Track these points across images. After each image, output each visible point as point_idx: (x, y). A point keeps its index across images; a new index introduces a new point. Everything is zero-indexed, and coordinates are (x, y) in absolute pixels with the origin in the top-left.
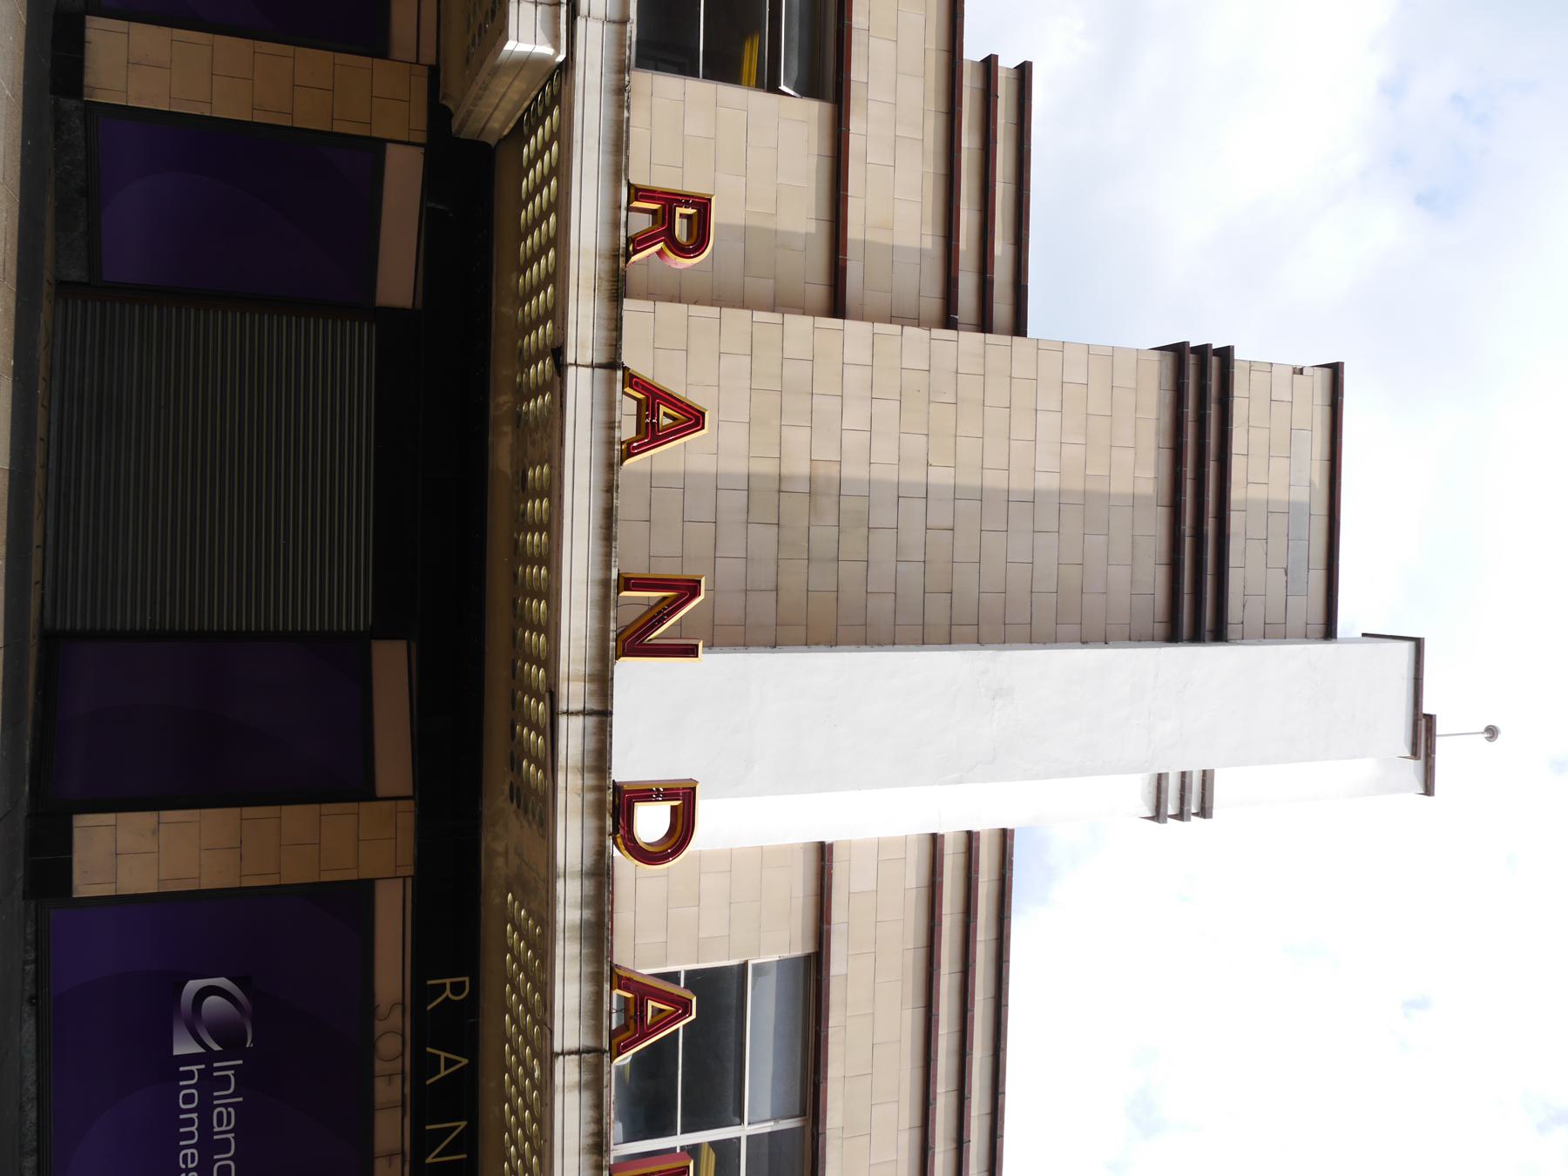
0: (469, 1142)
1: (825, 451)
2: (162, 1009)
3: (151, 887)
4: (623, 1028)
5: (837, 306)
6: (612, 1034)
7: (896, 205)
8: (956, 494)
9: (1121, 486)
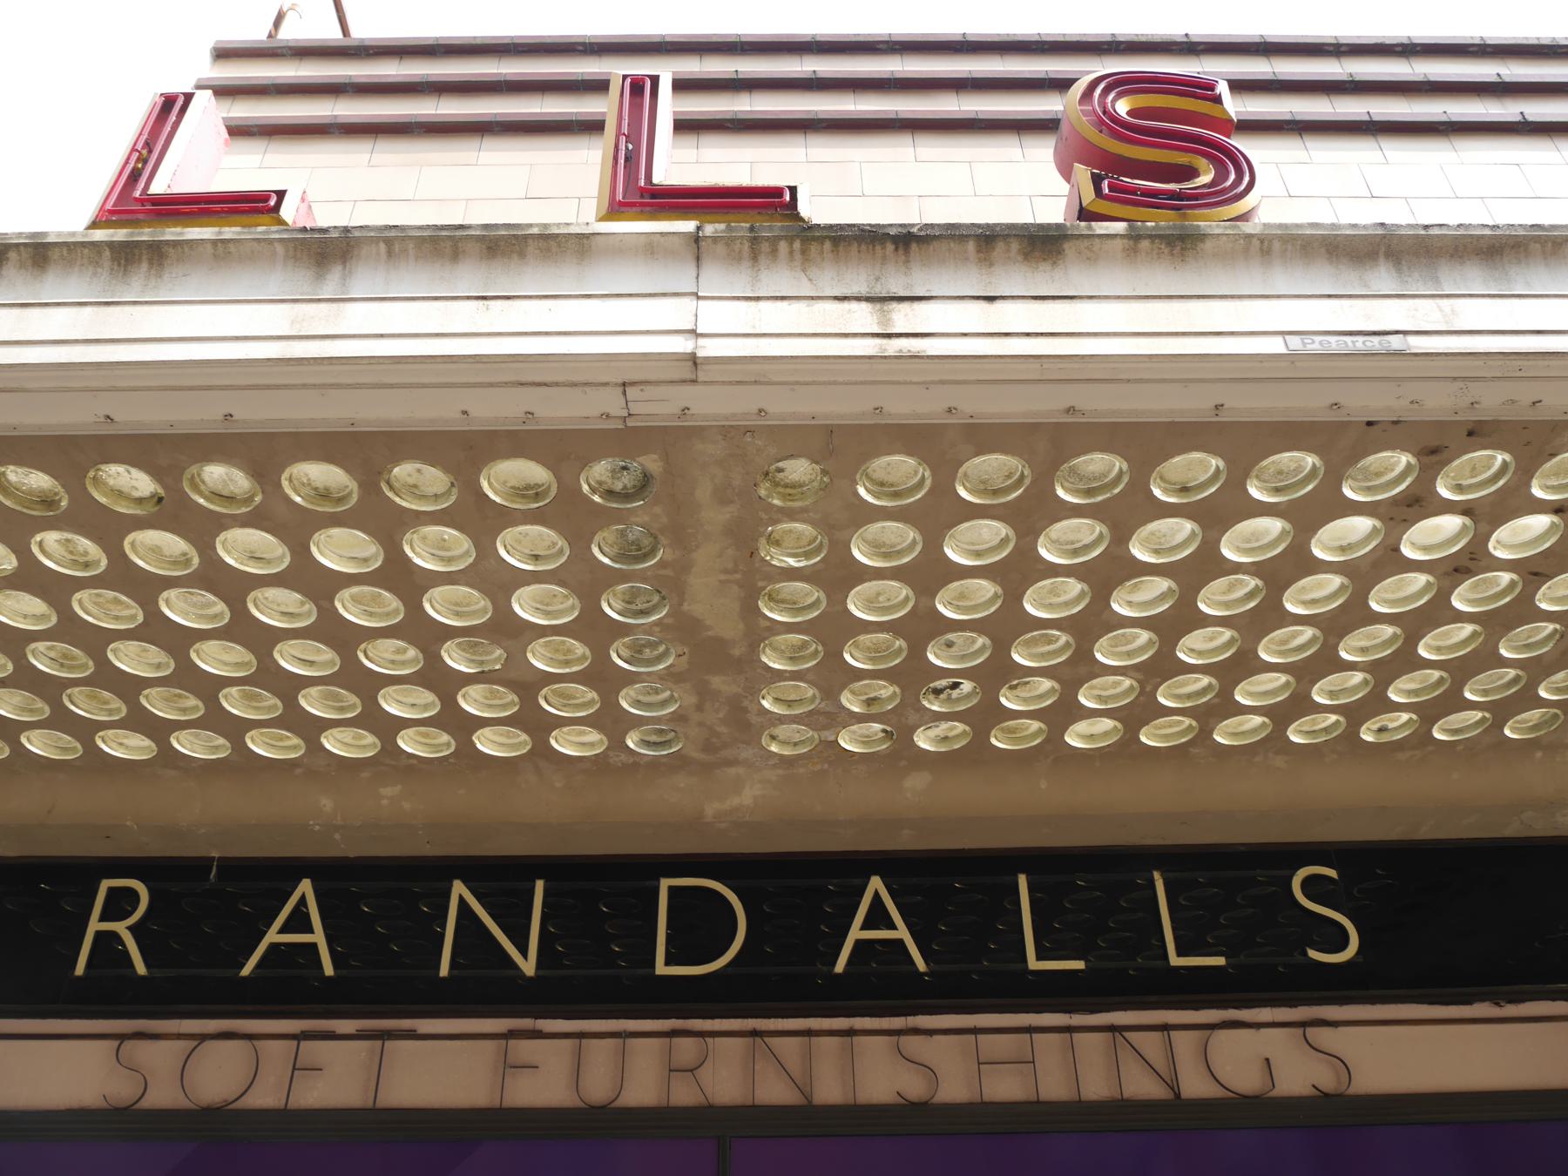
0: (502, 879)
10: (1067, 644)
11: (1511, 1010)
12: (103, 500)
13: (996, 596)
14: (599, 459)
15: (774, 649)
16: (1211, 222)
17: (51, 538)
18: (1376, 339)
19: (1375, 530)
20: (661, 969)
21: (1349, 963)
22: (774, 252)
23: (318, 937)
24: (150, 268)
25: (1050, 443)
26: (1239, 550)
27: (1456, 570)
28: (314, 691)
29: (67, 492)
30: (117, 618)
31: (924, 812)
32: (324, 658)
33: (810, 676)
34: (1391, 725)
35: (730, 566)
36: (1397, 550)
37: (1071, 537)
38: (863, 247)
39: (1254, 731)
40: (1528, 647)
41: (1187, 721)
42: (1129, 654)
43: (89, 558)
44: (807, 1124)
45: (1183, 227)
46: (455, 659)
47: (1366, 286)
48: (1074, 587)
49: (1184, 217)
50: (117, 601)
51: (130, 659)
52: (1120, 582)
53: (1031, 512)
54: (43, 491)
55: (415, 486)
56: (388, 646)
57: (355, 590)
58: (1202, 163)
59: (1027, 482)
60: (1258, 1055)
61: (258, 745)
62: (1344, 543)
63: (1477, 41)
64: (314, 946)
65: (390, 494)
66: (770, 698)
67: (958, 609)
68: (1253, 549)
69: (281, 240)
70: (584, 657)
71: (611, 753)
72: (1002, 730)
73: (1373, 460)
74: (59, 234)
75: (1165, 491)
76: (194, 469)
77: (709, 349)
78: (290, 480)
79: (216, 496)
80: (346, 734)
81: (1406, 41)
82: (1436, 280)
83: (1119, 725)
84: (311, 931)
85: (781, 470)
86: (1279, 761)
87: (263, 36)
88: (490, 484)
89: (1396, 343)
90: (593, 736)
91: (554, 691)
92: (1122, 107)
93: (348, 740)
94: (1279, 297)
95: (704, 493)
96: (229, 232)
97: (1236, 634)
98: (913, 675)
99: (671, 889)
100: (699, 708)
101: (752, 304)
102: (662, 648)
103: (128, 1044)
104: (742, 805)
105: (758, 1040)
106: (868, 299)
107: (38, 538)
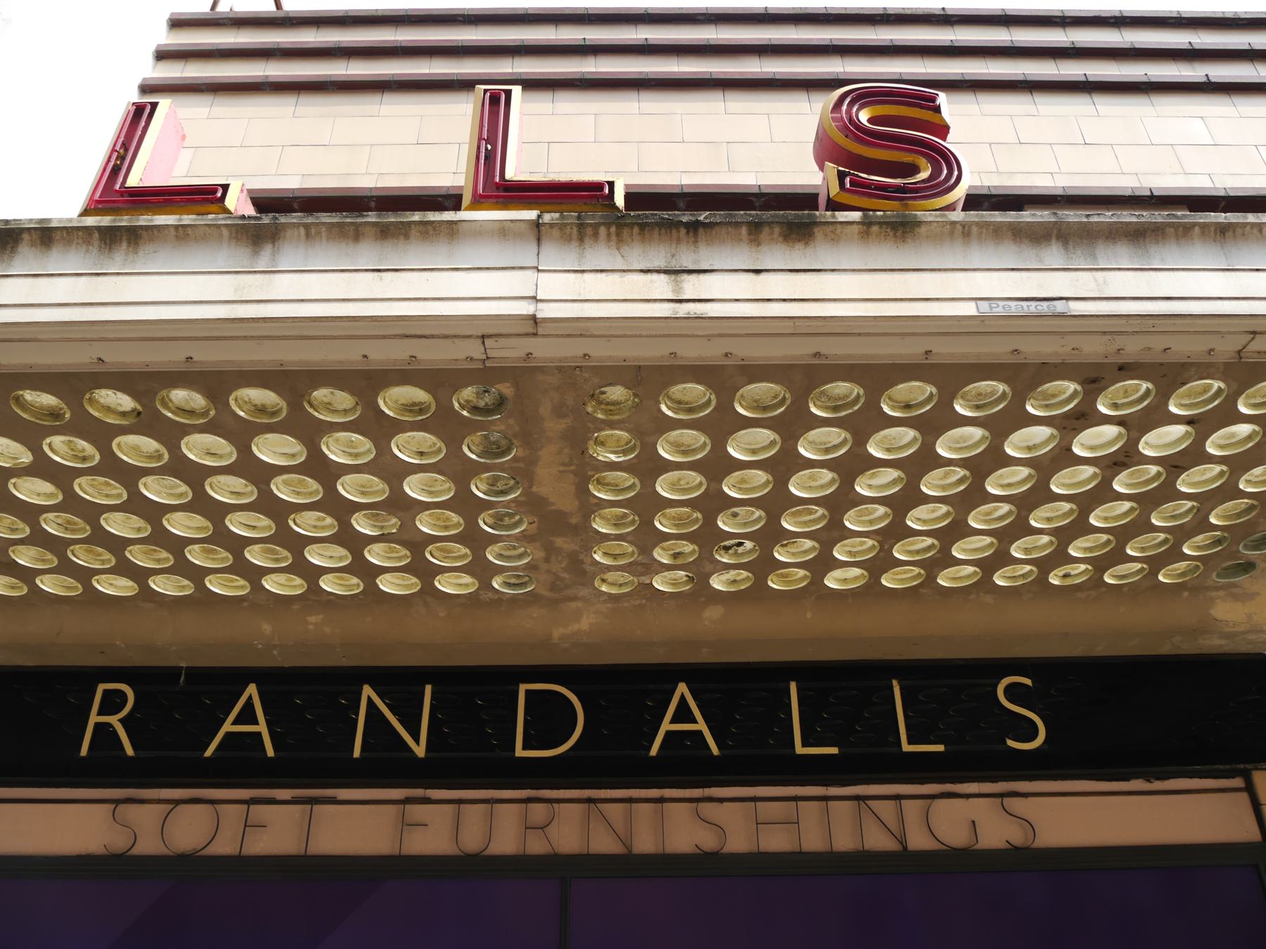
0: (400, 683)
10: (823, 516)
11: (1158, 785)
12: (96, 414)
13: (768, 482)
14: (466, 386)
15: (603, 518)
16: (925, 212)
17: (58, 440)
18: (1045, 304)
19: (1052, 437)
20: (520, 752)
21: (1037, 749)
22: (596, 235)
23: (262, 727)
24: (129, 246)
25: (805, 377)
26: (951, 449)
27: (1115, 464)
28: (257, 547)
29: (69, 408)
30: (107, 496)
31: (718, 635)
32: (264, 525)
33: (629, 538)
34: (1073, 573)
35: (567, 461)
36: (1070, 450)
37: (824, 439)
38: (663, 231)
39: (968, 576)
40: (1174, 517)
41: (917, 570)
42: (871, 522)
43: (86, 454)
44: (628, 867)
45: (904, 216)
46: (361, 524)
47: (1041, 261)
48: (827, 475)
49: (906, 207)
50: (108, 484)
51: (117, 525)
52: (862, 472)
53: (792, 424)
54: (51, 407)
55: (329, 404)
56: (311, 517)
57: (285, 477)
58: (922, 162)
59: (788, 402)
60: (969, 818)
61: (215, 585)
62: (1031, 444)
63: (1175, 15)
64: (259, 734)
65: (311, 410)
66: (600, 553)
67: (740, 490)
68: (961, 448)
69: (226, 225)
70: (459, 524)
71: (481, 592)
72: (778, 575)
73: (1049, 387)
74: (60, 220)
75: (893, 408)
76: (164, 393)
77: (546, 311)
78: (236, 400)
79: (180, 410)
80: (282, 578)
81: (1117, 15)
82: (1094, 257)
83: (865, 573)
84: (255, 722)
85: (604, 393)
86: (988, 599)
87: (207, 9)
88: (385, 402)
89: (1060, 307)
90: (467, 579)
91: (437, 548)
92: (864, 116)
93: (283, 581)
94: (974, 270)
95: (545, 409)
96: (188, 219)
97: (951, 509)
98: (708, 537)
99: (527, 692)
100: (547, 560)
101: (579, 275)
102: (517, 518)
103: (122, 807)
104: (580, 629)
105: (592, 805)
106: (666, 272)
107: (48, 440)
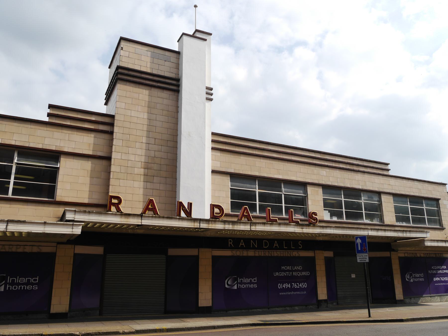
0: (254, 240)
1: (139, 165)
2: (230, 291)
3: (211, 293)
4: (248, 219)
5: (108, 159)
6: (248, 220)
7: (84, 142)
8: (148, 137)
9: (147, 98)
